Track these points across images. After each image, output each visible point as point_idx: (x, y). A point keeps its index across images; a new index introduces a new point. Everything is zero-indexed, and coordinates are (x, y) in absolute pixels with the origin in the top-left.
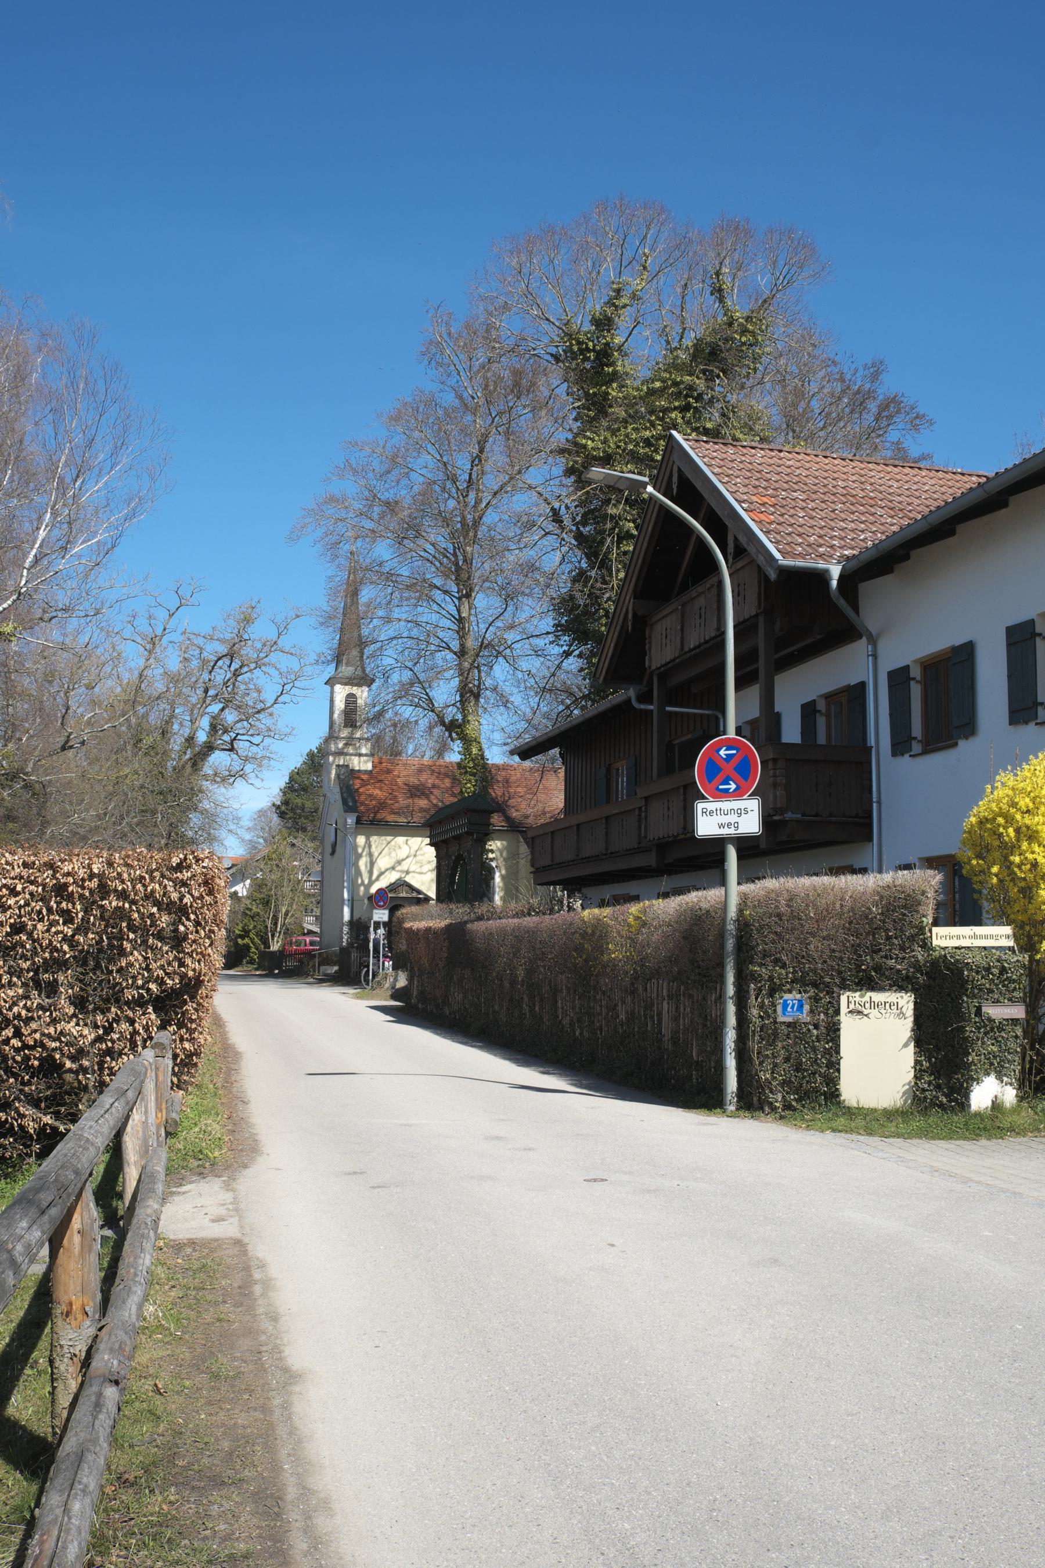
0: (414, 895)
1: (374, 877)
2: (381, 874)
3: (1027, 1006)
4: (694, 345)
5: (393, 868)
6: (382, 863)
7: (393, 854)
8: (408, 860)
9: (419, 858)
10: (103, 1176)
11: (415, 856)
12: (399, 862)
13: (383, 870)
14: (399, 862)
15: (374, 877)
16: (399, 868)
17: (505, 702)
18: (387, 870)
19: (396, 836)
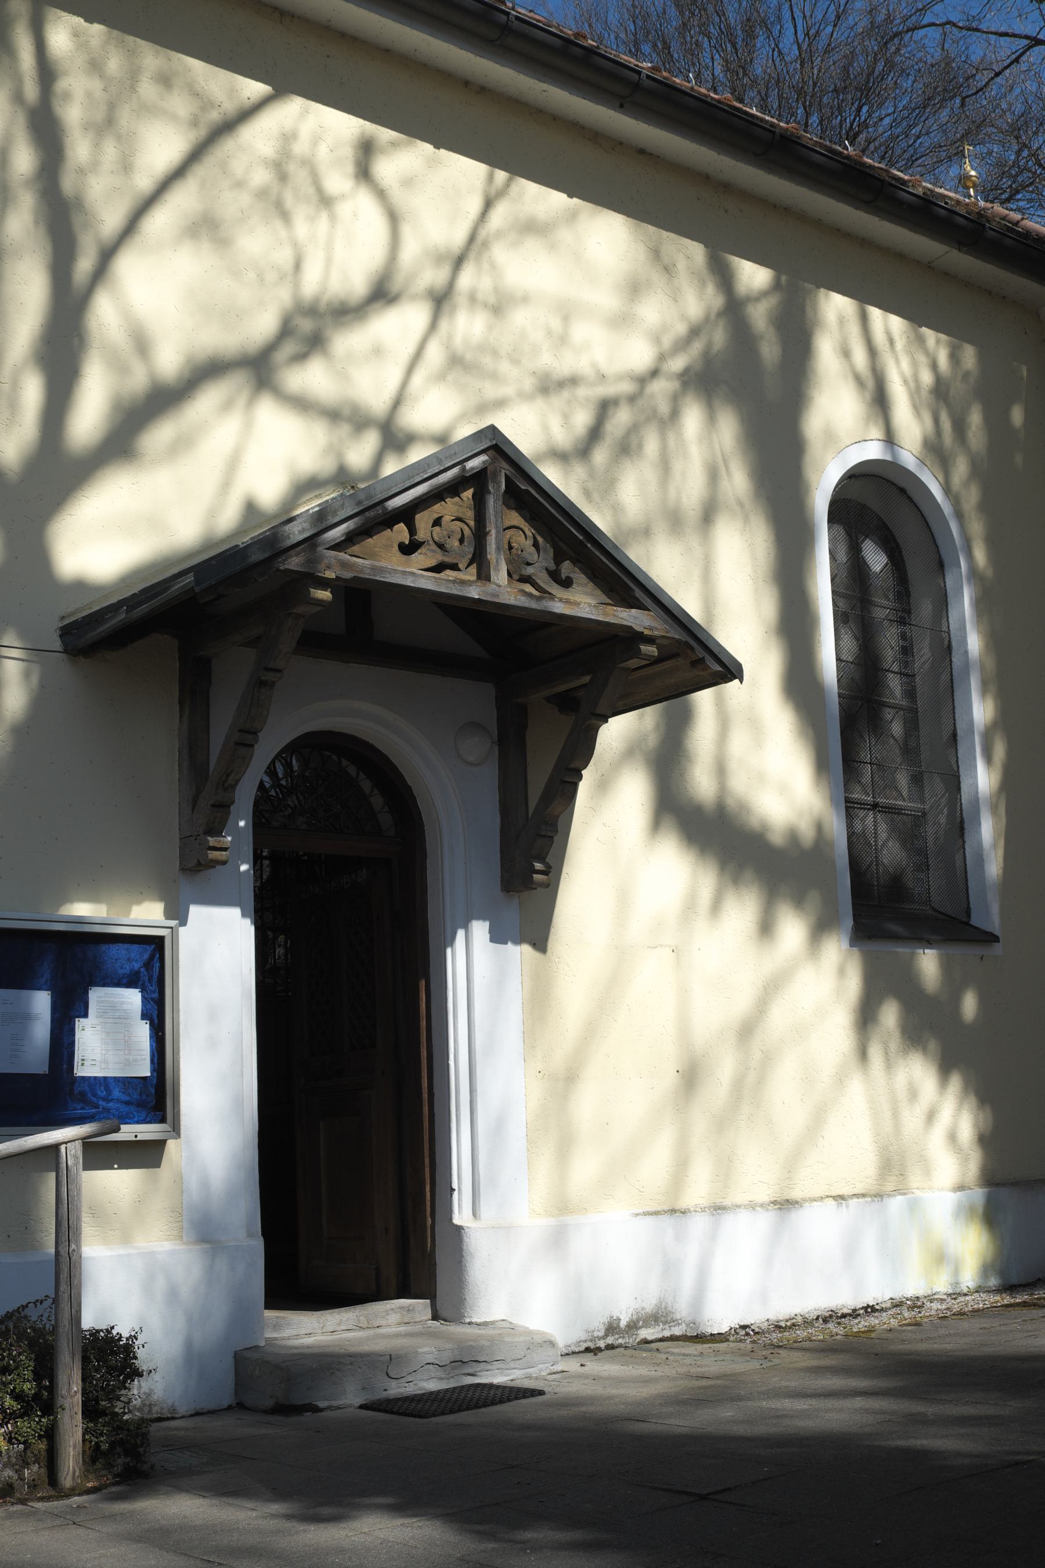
0: (582, 602)
1: (89, 417)
2: (161, 400)
3: (818, 287)
4: (112, 1338)
5: (258, 369)
6: (160, 298)
7: (258, 242)
8: (400, 325)
9: (467, 326)
10: (364, 119)
11: (441, 300)
12: (310, 328)
13: (169, 361)
14: (310, 328)
15: (89, 417)
16: (312, 378)
17: (233, 464)
18: (205, 372)
19: (284, 84)
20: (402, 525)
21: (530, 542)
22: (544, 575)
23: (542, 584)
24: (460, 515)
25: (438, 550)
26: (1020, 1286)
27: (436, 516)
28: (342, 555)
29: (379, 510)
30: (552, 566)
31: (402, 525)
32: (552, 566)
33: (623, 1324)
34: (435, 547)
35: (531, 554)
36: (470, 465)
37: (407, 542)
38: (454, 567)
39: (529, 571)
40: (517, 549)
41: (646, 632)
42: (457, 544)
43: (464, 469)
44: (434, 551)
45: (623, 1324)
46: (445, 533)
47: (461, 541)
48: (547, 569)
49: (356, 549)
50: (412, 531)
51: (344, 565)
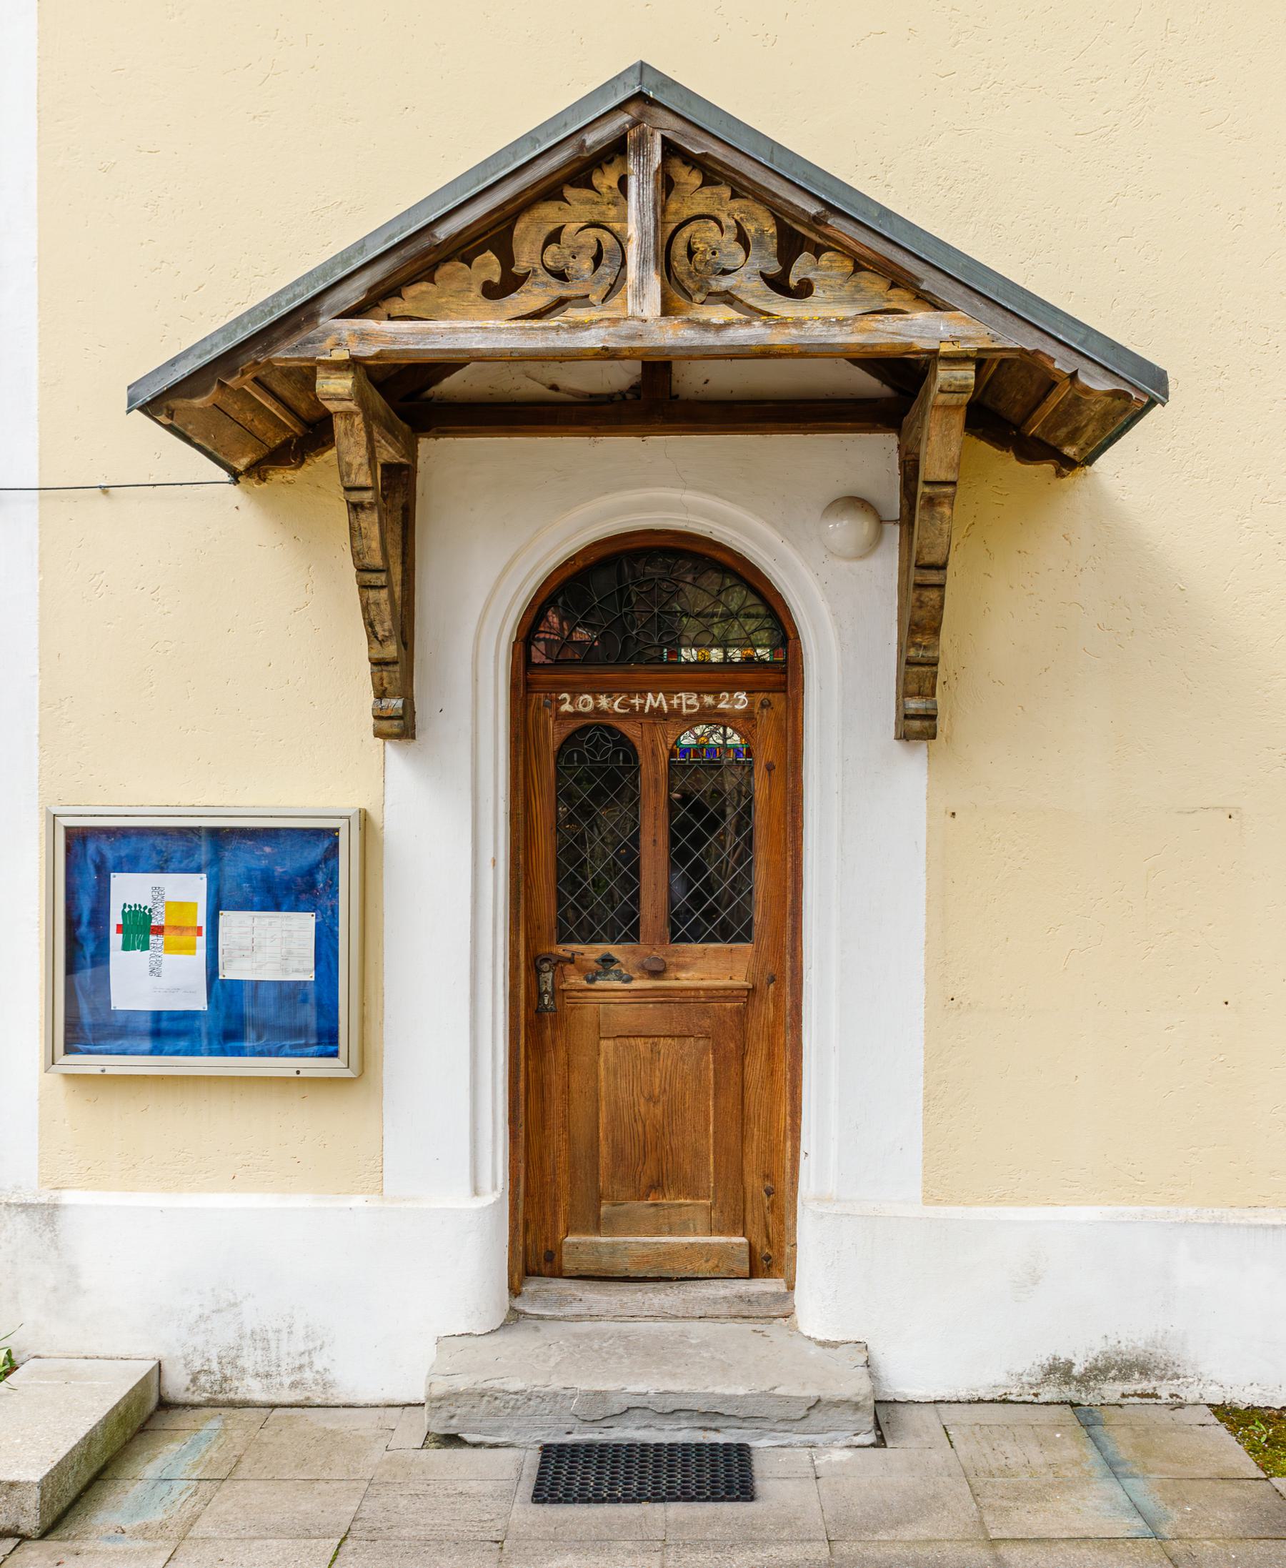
20: (489, 254)
21: (730, 236)
22: (758, 285)
23: (751, 301)
24: (597, 218)
25: (553, 280)
26: (88, 1487)
27: (551, 228)
28: (368, 324)
29: (424, 243)
30: (774, 268)
31: (489, 254)
32: (774, 268)
33: (1077, 1370)
34: (548, 278)
35: (730, 255)
36: (591, 138)
37: (496, 279)
38: (583, 300)
39: (725, 283)
40: (704, 253)
41: (945, 348)
42: (587, 264)
43: (582, 146)
44: (546, 284)
45: (1077, 1370)
46: (567, 252)
47: (597, 260)
48: (762, 275)
49: (396, 306)
50: (507, 259)
51: (363, 336)
